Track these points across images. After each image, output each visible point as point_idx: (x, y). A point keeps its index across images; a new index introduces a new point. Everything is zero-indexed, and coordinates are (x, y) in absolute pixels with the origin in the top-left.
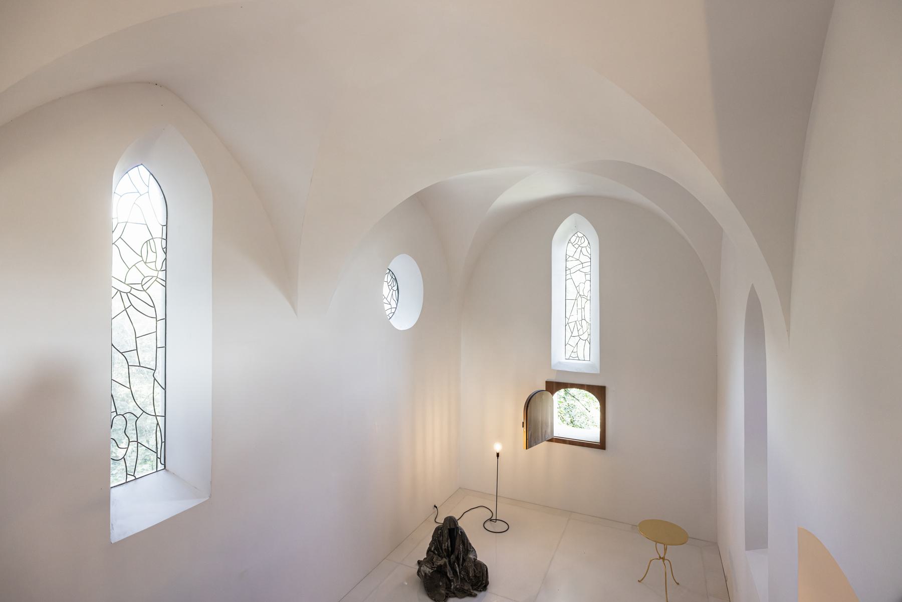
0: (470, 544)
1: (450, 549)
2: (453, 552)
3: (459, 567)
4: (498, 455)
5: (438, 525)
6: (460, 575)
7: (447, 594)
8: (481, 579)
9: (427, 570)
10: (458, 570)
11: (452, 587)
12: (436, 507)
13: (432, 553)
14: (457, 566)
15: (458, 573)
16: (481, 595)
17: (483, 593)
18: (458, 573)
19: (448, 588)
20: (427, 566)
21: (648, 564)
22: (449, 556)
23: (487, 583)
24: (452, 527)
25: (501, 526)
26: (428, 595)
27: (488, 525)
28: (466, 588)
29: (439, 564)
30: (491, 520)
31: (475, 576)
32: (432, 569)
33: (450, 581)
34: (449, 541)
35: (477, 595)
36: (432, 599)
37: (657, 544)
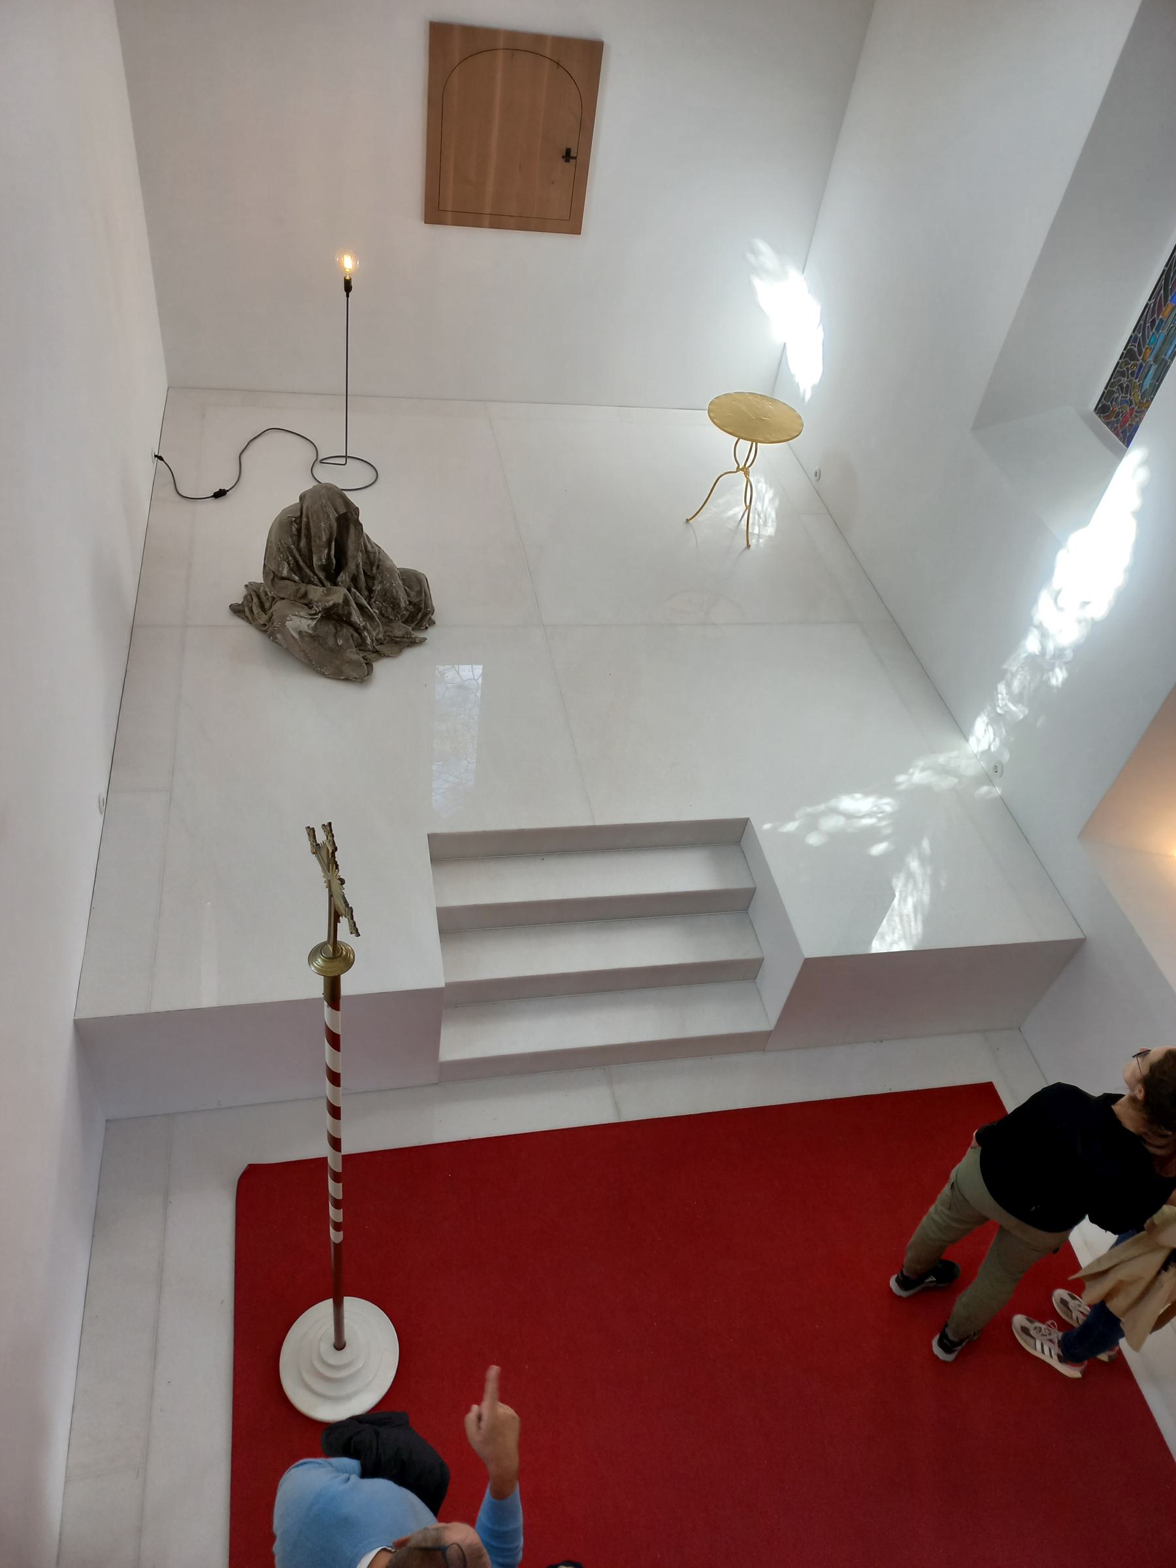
0: (367, 536)
4: (348, 287)
11: (369, 641)
16: (430, 634)
19: (361, 645)
24: (342, 510)
26: (323, 675)
29: (331, 603)
31: (410, 603)
32: (312, 619)
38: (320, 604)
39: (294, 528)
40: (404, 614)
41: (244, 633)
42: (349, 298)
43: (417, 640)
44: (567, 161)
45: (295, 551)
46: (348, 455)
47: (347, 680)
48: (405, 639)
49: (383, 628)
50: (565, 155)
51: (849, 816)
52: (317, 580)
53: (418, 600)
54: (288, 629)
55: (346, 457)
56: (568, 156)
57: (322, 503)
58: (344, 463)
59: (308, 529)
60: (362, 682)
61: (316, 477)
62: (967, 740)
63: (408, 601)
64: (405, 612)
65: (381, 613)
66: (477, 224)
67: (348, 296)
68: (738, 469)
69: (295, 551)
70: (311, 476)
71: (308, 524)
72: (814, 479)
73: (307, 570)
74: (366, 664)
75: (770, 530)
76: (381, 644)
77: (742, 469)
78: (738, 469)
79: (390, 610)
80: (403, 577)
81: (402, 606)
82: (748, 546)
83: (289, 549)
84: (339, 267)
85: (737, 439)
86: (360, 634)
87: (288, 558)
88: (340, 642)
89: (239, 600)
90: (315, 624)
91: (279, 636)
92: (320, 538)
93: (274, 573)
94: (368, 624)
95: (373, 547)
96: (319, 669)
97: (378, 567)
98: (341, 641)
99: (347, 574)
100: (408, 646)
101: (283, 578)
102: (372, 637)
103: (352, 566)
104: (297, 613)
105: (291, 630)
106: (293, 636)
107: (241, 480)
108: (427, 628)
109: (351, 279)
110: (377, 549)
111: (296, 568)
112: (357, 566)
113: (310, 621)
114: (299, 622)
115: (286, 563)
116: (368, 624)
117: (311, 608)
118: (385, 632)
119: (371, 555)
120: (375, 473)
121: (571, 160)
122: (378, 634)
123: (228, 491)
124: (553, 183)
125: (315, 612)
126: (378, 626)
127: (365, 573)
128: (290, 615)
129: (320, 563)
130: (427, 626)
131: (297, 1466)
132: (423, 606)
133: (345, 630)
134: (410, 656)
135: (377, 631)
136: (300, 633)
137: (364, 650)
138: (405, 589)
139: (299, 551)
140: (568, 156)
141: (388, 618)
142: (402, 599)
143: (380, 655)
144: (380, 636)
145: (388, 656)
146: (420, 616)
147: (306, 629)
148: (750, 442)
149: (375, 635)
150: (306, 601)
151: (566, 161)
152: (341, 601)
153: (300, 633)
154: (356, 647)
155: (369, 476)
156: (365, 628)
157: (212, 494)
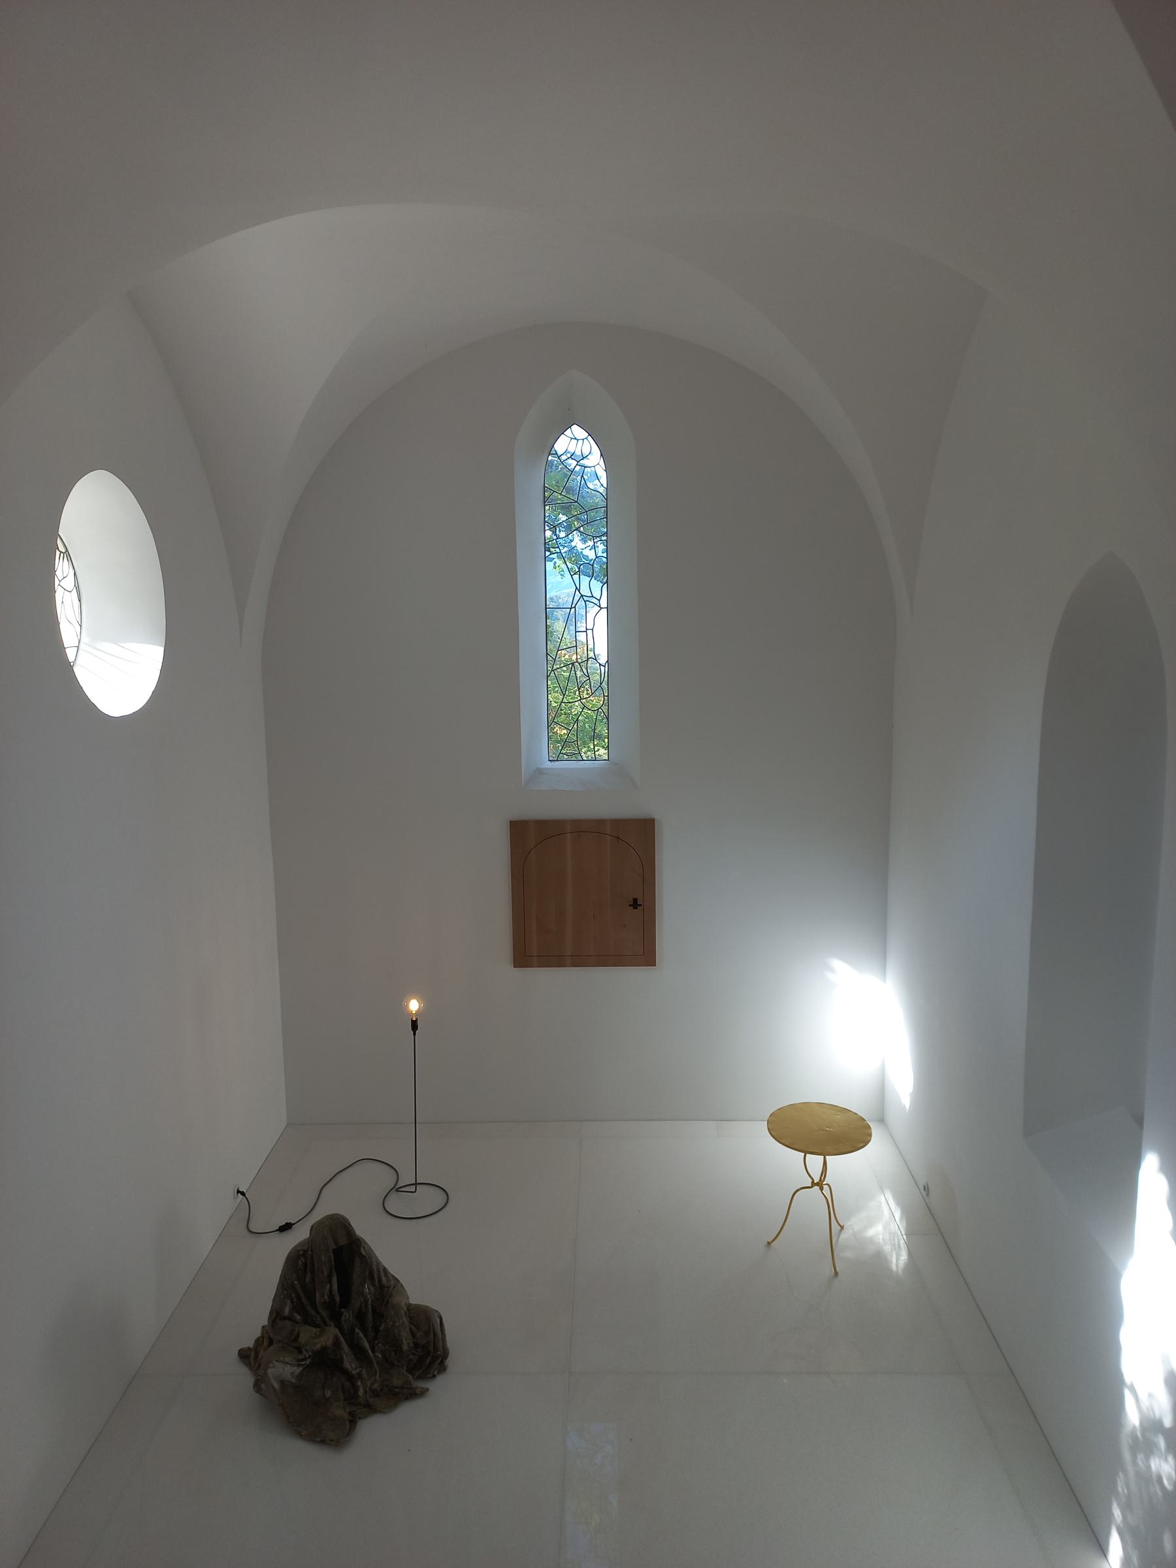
0: (385, 1270)
1: (338, 1298)
2: (346, 1300)
3: (366, 1336)
4: (414, 1025)
5: (1162, 1463)
6: (375, 1356)
7: (350, 1413)
8: (431, 1349)
9: (284, 1369)
10: (366, 1345)
11: (361, 1392)
12: (243, 1194)
13: (288, 1323)
14: (361, 1335)
15: (370, 1352)
16: (438, 1386)
17: (441, 1380)
18: (370, 1352)
19: (351, 1398)
20: (281, 1362)
21: (387, 1192)
22: (336, 1318)
23: (446, 1354)
24: (343, 1241)
25: (428, 1199)
26: (299, 1435)
27: (394, 1204)
28: (396, 1382)
29: (318, 1346)
30: (397, 1189)
31: (416, 1345)
32: (299, 1365)
33: (350, 1378)
34: (335, 1279)
35: (428, 1390)
36: (314, 1441)
37: (808, 1155)
39: (300, 1262)
41: (244, 1377)
42: (416, 1036)
43: (418, 1391)
44: (635, 908)
46: (418, 1182)
47: (323, 1442)
48: (404, 1390)
49: (380, 1376)
50: (632, 904)
52: (319, 1319)
53: (425, 1342)
54: (269, 1378)
55: (416, 1184)
56: (635, 904)
58: (414, 1190)
61: (386, 1208)
63: (414, 1343)
64: (412, 1356)
66: (561, 964)
67: (414, 1034)
68: (813, 1184)
70: (383, 1209)
71: (312, 1257)
72: (924, 1193)
73: (309, 1308)
75: (904, 1256)
77: (817, 1184)
78: (813, 1184)
79: (393, 1353)
81: (404, 1350)
82: (836, 1274)
84: (404, 1009)
89: (250, 1343)
90: (300, 1373)
91: (263, 1386)
92: (322, 1272)
94: (364, 1372)
95: (389, 1281)
98: (329, 1392)
99: (351, 1312)
101: (285, 1318)
104: (282, 1359)
106: (272, 1386)
108: (434, 1376)
109: (417, 1019)
110: (392, 1283)
113: (295, 1368)
116: (364, 1372)
117: (300, 1352)
120: (442, 1192)
121: (638, 907)
122: (373, 1384)
123: (294, 1224)
124: (625, 926)
125: (304, 1357)
126: (375, 1374)
127: (374, 1311)
128: (274, 1362)
130: (436, 1373)
132: (431, 1349)
134: (407, 1410)
135: (372, 1380)
136: (282, 1382)
140: (635, 904)
142: (404, 1341)
143: (371, 1409)
144: (376, 1386)
148: (803, 1154)
149: (369, 1385)
151: (634, 908)
152: (329, 1343)
153: (282, 1382)
155: (437, 1199)
156: (360, 1375)
157: (277, 1228)
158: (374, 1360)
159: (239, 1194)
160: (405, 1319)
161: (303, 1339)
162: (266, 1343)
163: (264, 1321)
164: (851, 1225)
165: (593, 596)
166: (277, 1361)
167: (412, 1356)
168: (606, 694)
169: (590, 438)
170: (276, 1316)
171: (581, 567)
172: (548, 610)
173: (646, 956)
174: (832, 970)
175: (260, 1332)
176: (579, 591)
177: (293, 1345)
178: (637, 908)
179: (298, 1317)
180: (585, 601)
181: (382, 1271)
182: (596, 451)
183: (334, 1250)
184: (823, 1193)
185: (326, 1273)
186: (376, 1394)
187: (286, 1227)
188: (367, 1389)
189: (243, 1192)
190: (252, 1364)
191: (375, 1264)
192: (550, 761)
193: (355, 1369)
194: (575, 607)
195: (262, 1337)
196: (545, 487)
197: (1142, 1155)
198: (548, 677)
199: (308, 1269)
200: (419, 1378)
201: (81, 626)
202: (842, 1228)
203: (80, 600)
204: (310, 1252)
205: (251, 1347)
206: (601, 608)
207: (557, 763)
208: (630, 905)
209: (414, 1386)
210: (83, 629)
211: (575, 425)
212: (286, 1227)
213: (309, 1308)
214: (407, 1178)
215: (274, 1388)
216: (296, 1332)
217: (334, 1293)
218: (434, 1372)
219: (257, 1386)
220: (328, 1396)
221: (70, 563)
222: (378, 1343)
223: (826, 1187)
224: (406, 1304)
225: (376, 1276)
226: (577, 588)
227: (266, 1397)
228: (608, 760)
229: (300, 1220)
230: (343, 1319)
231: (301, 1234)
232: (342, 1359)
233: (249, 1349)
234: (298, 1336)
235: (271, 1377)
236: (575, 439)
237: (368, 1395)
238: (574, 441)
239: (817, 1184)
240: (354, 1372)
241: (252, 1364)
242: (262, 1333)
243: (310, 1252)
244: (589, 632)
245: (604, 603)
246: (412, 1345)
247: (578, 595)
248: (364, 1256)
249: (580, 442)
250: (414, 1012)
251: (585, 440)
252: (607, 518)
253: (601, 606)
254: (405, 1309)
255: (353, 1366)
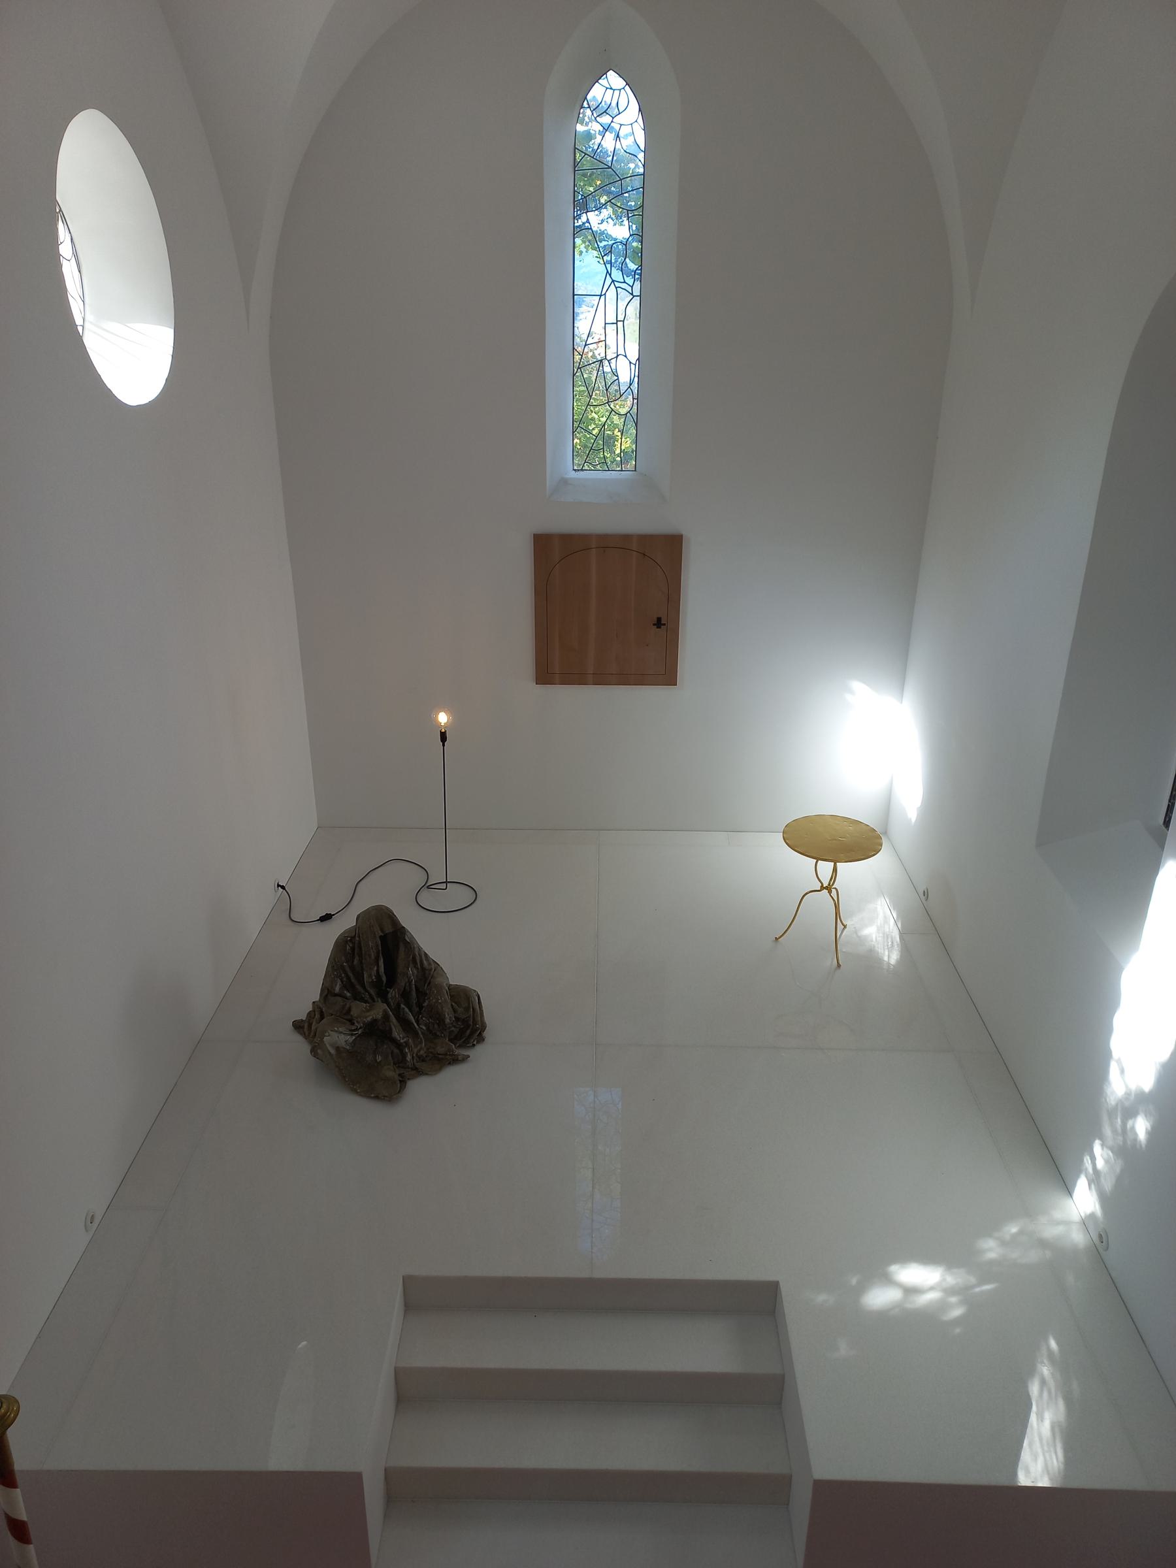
0: (426, 954)
1: (384, 979)
2: (392, 981)
4: (443, 737)
7: (400, 1075)
9: (338, 1038)
10: (411, 1018)
11: (409, 1058)
12: (283, 887)
13: (339, 999)
14: (407, 1010)
15: (416, 1025)
16: (478, 1054)
17: (479, 1049)
18: (416, 1025)
19: (400, 1062)
20: (336, 1031)
22: (383, 996)
23: (484, 1027)
24: (389, 929)
25: (457, 896)
26: (355, 1091)
28: (440, 1050)
29: (369, 1019)
31: (457, 1019)
32: (352, 1035)
33: (399, 1046)
38: (359, 1020)
40: (453, 1031)
41: (300, 1046)
43: (460, 1058)
45: (348, 969)
47: (377, 1098)
49: (425, 1045)
51: (911, 1291)
54: (325, 1045)
55: (446, 882)
56: (659, 623)
57: (371, 923)
59: (360, 948)
60: (390, 1101)
61: (419, 903)
62: (1069, 1191)
63: (455, 1017)
64: (453, 1029)
65: (428, 1029)
67: (444, 745)
68: (822, 888)
69: (348, 969)
71: (360, 943)
72: (923, 898)
73: (358, 987)
74: (400, 1081)
76: (423, 1061)
77: (826, 888)
78: (822, 888)
79: (436, 1026)
80: (452, 994)
81: (446, 1023)
82: (839, 966)
83: (342, 967)
85: (815, 860)
86: (402, 1051)
87: (341, 976)
88: (379, 1058)
91: (319, 1051)
92: (370, 956)
93: (328, 990)
95: (430, 964)
96: (352, 1086)
97: (429, 983)
100: (449, 1063)
101: (336, 995)
102: (413, 1053)
103: (402, 982)
104: (336, 1029)
105: (328, 1046)
107: (423, 909)
108: (474, 1045)
109: (446, 731)
110: (433, 967)
111: (348, 985)
112: (410, 982)
114: (338, 1038)
115: (339, 980)
118: (428, 1049)
119: (427, 972)
120: (474, 893)
122: (419, 1051)
123: (334, 915)
126: (421, 1043)
129: (370, 980)
130: (475, 1043)
131: (1095, 1203)
133: (385, 1046)
134: (450, 1074)
135: (419, 1048)
136: (338, 1049)
137: (403, 1067)
138: (452, 1005)
139: (352, 968)
140: (659, 623)
141: (435, 1034)
142: (447, 1016)
143: (418, 1072)
144: (422, 1052)
145: (427, 1074)
146: (468, 1032)
147: (343, 1044)
150: (349, 1017)
151: (657, 628)
152: (379, 1017)
153: (338, 1049)
154: (394, 1064)
155: (468, 896)
156: (407, 1043)
158: (420, 1033)
159: (280, 888)
160: (447, 996)
161: (355, 1012)
162: (317, 1016)
163: (316, 997)
164: (853, 925)
165: (625, 282)
166: (332, 1031)
167: (453, 1029)
168: (636, 396)
169: (627, 88)
170: (327, 992)
171: (608, 251)
172: (575, 297)
173: (668, 677)
174: (851, 692)
175: (311, 1006)
176: (610, 275)
177: (346, 1017)
178: (660, 628)
179: (348, 994)
180: (616, 288)
181: (423, 956)
182: (634, 105)
183: (380, 937)
184: (831, 896)
185: (373, 957)
186: (422, 1059)
187: (326, 918)
188: (414, 1055)
189: (283, 886)
190: (307, 1034)
191: (417, 950)
192: (575, 470)
193: (403, 1039)
194: (605, 294)
195: (314, 1011)
196: (575, 148)
197: (1162, 864)
198: (574, 375)
199: (356, 954)
200: (460, 1046)
201: (83, 302)
202: (845, 927)
203: (79, 271)
204: (357, 939)
205: (304, 1019)
206: (634, 296)
207: (581, 472)
208: (654, 625)
209: (456, 1053)
210: (86, 306)
211: (611, 71)
212: (326, 918)
213: (358, 987)
214: (437, 876)
215: (330, 1053)
216: (348, 1006)
217: (380, 974)
218: (474, 1041)
219: (314, 1051)
220: (378, 1061)
221: (66, 226)
222: (422, 1018)
223: (833, 890)
224: (447, 984)
225: (418, 961)
226: (608, 272)
227: (322, 1061)
228: (635, 470)
229: (340, 911)
230: (389, 996)
231: (346, 922)
232: (391, 1029)
233: (302, 1020)
234: (349, 1010)
235: (326, 1043)
236: (611, 89)
237: (415, 1060)
238: (610, 92)
239: (826, 888)
240: (402, 1041)
241: (307, 1034)
242: (313, 1007)
243: (357, 939)
244: (620, 324)
245: (637, 292)
246: (454, 1019)
247: (609, 281)
248: (409, 943)
249: (617, 93)
250: (443, 724)
251: (622, 91)
252: (643, 188)
253: (634, 294)
254: (447, 988)
255: (401, 1036)
